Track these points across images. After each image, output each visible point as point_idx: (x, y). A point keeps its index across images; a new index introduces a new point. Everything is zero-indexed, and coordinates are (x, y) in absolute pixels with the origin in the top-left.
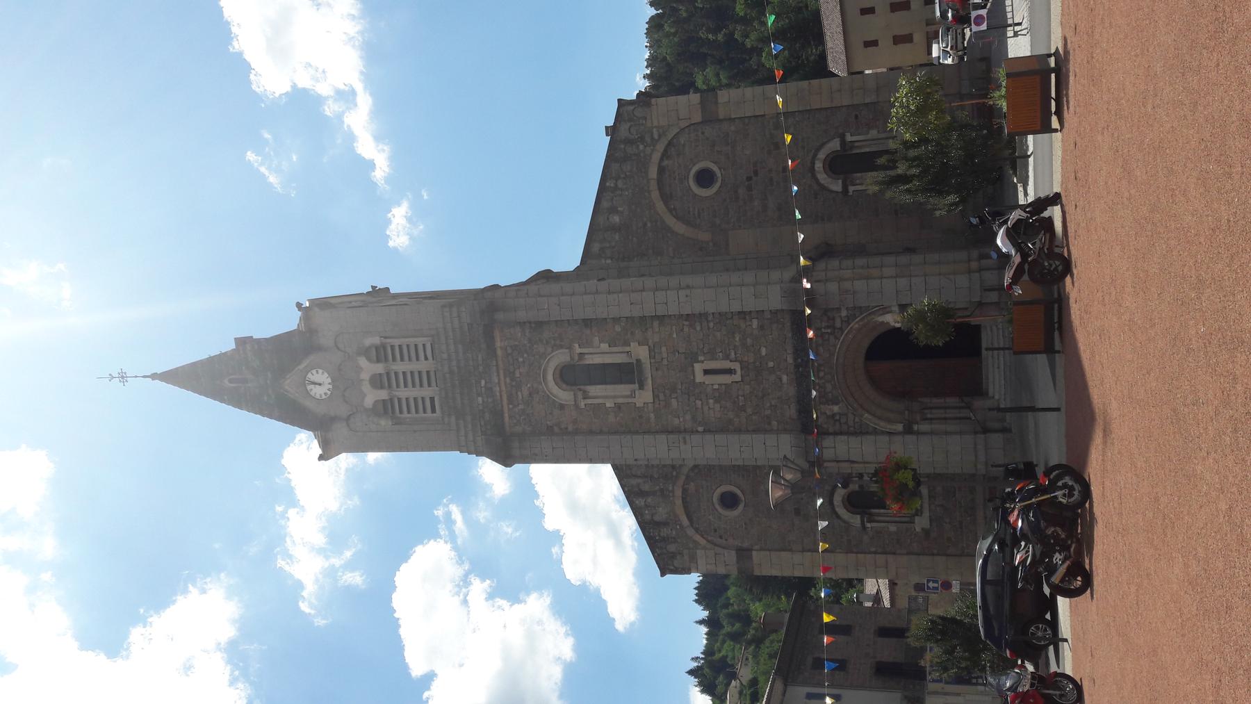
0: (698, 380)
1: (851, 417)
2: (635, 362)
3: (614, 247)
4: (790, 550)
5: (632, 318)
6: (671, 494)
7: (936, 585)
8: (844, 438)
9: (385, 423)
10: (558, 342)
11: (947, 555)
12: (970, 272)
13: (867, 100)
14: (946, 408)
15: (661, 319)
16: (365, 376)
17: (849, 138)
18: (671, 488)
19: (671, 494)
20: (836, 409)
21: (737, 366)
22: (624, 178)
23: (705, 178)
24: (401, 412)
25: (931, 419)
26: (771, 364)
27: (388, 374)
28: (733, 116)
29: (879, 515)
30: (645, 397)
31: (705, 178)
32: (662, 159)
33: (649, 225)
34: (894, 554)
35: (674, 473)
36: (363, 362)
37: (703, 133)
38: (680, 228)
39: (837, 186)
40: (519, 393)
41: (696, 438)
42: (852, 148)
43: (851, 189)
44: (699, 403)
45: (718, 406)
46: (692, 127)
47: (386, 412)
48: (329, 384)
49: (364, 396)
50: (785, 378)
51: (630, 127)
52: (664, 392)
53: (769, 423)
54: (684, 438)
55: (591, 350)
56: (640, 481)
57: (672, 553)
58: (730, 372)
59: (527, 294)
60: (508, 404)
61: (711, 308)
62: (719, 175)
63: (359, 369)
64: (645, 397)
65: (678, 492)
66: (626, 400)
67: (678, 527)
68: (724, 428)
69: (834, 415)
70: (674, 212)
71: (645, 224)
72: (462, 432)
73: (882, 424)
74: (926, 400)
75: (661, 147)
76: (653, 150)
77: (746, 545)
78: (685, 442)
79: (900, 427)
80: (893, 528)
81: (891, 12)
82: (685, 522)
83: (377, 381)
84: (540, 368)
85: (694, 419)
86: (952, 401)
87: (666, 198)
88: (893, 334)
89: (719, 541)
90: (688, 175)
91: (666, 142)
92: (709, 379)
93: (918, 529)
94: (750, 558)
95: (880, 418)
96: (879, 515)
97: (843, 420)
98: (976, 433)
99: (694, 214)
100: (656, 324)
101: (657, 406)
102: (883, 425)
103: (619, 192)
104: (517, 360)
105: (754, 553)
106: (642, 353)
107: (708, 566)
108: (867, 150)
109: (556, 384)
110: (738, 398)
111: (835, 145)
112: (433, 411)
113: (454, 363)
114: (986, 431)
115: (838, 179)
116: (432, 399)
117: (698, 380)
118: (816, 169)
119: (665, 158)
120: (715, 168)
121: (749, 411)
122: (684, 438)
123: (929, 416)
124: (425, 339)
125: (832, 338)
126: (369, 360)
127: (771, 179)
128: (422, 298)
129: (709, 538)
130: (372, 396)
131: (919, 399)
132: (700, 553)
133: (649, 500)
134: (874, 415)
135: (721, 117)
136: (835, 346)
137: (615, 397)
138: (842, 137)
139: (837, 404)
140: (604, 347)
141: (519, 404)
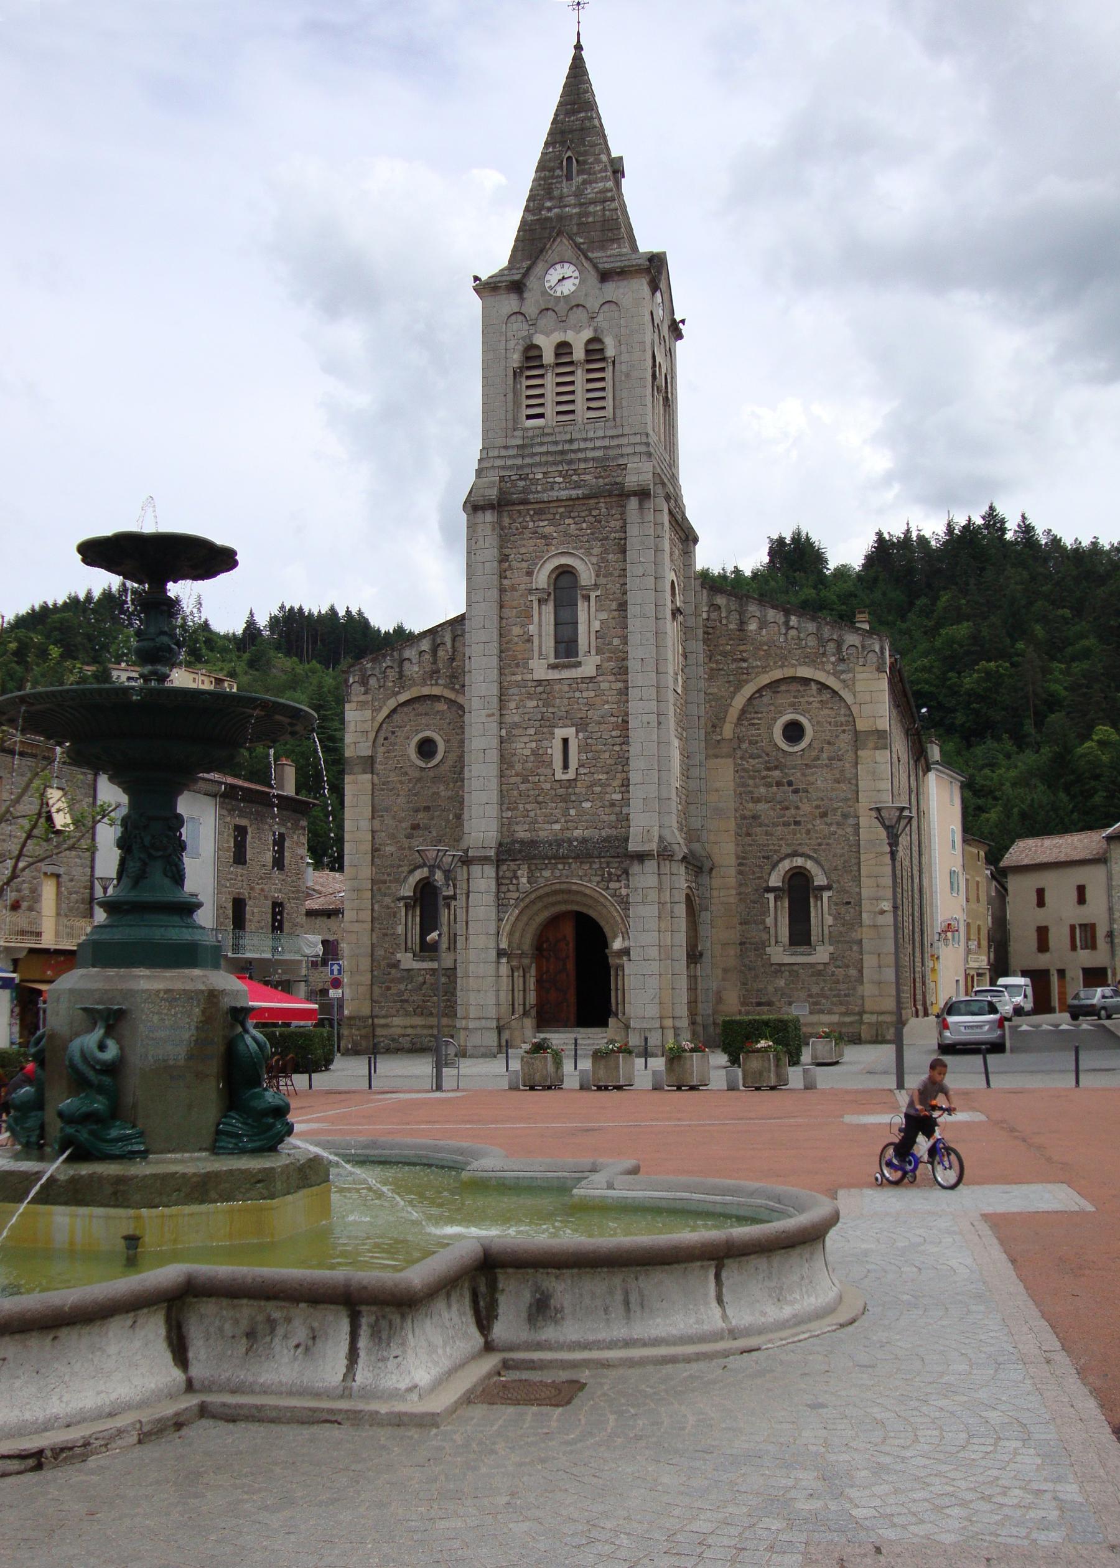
0: (557, 730)
1: (515, 895)
2: (578, 659)
3: (720, 622)
4: (373, 818)
5: (625, 659)
6: (433, 682)
7: (336, 972)
8: (493, 888)
9: (516, 359)
10: (603, 571)
11: (372, 984)
12: (661, 1018)
13: (864, 915)
14: (524, 990)
15: (624, 692)
16: (569, 336)
17: (826, 895)
18: (440, 682)
19: (433, 682)
20: (524, 880)
21: (571, 774)
22: (799, 637)
23: (794, 732)
24: (528, 377)
25: (513, 976)
26: (572, 812)
27: (571, 363)
28: (859, 766)
29: (413, 916)
30: (539, 669)
31: (794, 732)
32: (818, 682)
33: (745, 665)
34: (372, 930)
35: (457, 687)
36: (587, 334)
37: (844, 731)
38: (739, 701)
39: (775, 880)
40: (546, 523)
41: (494, 726)
42: (816, 897)
43: (771, 896)
44: (532, 731)
45: (528, 752)
46: (851, 719)
47: (528, 359)
48: (562, 293)
49: (547, 334)
50: (557, 827)
51: (857, 647)
52: (544, 692)
53: (508, 809)
54: (493, 715)
55: (593, 609)
56: (449, 645)
57: (368, 682)
58: (566, 766)
59: (658, 537)
60: (534, 509)
61: (634, 749)
62: (796, 749)
63: (578, 329)
64: (539, 669)
65: (436, 691)
66: (536, 649)
67: (397, 689)
68: (505, 761)
69: (517, 878)
70: (757, 695)
71: (744, 660)
72: (504, 453)
73: (508, 927)
74: (533, 972)
75: (831, 682)
76: (828, 672)
77: (378, 767)
78: (489, 716)
79: (504, 945)
80: (400, 929)
81: (1094, 924)
82: (403, 698)
83: (563, 348)
84: (574, 548)
85: (515, 725)
86: (532, 998)
87: (774, 685)
88: (602, 941)
89: (382, 735)
90: (798, 713)
91: (836, 689)
92: (558, 745)
93: (399, 956)
94: (364, 772)
95: (514, 925)
96: (413, 916)
97: (511, 887)
98: (498, 1019)
99: (754, 718)
100: (620, 685)
101: (530, 684)
102: (506, 927)
103: (784, 631)
104: (584, 521)
105: (369, 776)
106: (588, 669)
107: (353, 724)
108: (813, 914)
109: (557, 568)
110: (537, 775)
111: (820, 880)
112: (529, 417)
113: (582, 445)
114: (500, 1030)
115: (783, 882)
116: (541, 416)
117: (557, 730)
118: (795, 858)
119: (819, 686)
120: (803, 744)
121: (523, 787)
122: (493, 715)
123: (516, 974)
124: (611, 410)
125: (599, 878)
126: (590, 341)
127: (787, 809)
128: (667, 392)
129: (384, 725)
130: (547, 344)
131: (534, 965)
132: (368, 714)
133: (427, 656)
134: (517, 919)
135: (860, 753)
136: (590, 881)
137: (540, 636)
138: (828, 888)
139: (529, 882)
140: (596, 625)
141: (534, 521)
